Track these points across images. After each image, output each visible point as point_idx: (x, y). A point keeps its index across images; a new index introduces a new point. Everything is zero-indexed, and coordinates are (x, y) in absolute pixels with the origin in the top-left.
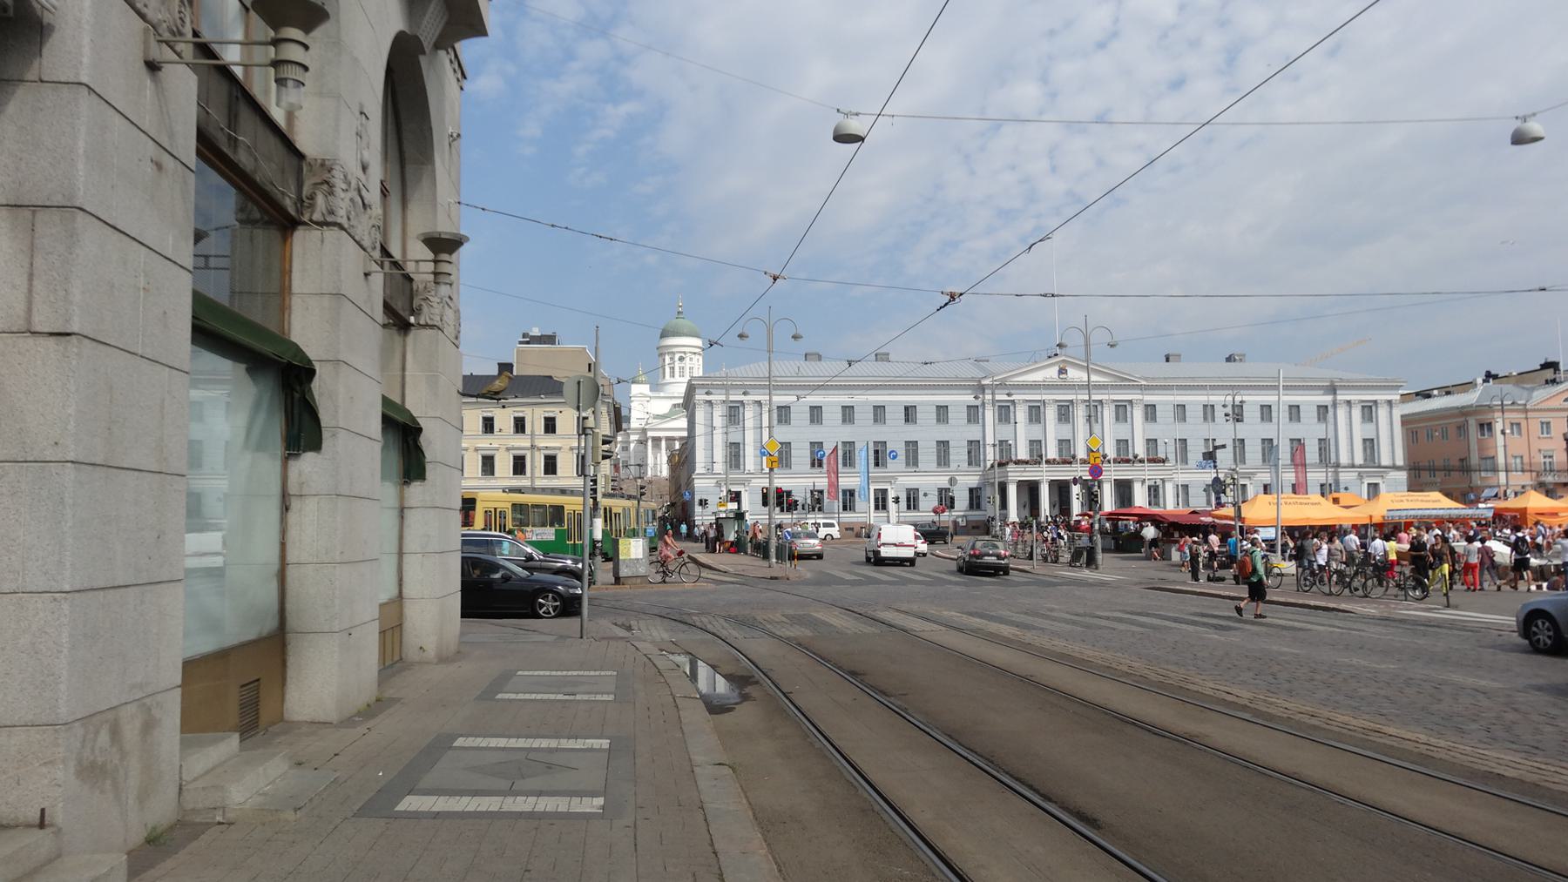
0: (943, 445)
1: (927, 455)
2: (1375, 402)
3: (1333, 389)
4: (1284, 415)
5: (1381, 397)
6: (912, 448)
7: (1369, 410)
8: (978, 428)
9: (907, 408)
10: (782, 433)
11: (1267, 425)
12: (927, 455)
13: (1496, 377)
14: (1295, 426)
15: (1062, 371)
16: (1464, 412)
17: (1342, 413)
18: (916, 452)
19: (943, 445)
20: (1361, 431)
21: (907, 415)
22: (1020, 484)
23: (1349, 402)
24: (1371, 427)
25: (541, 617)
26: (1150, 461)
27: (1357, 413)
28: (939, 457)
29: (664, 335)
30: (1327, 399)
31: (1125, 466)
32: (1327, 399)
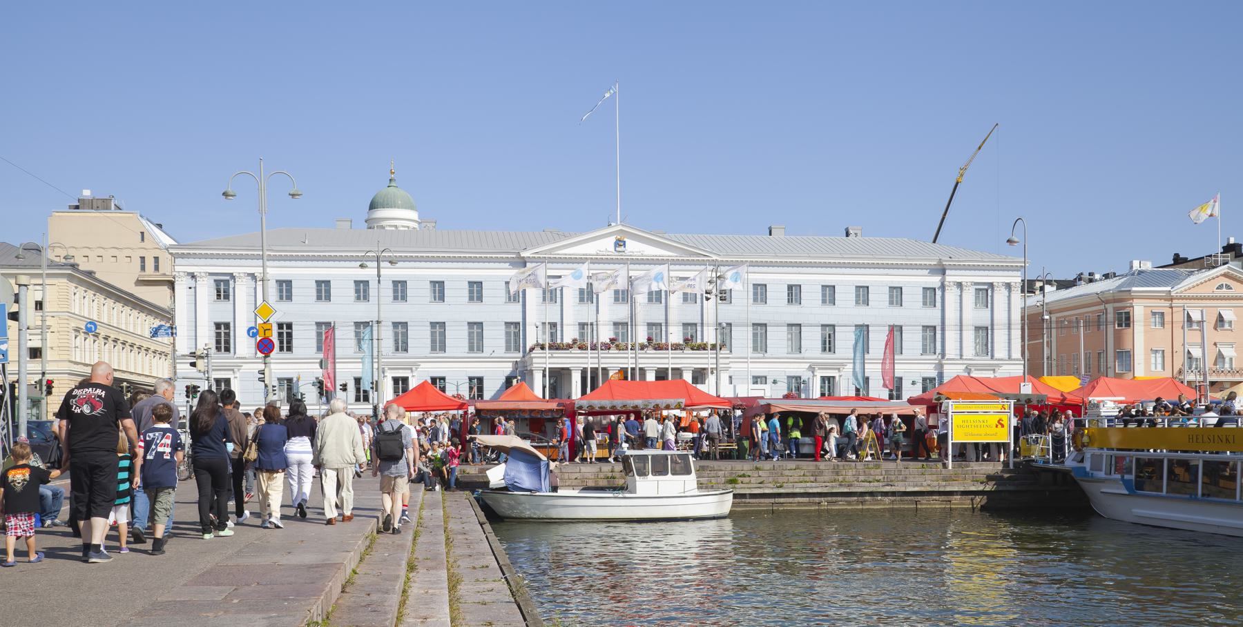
0: (476, 327)
1: (457, 338)
2: (991, 285)
3: (942, 271)
4: (388, 290)
5: (998, 278)
6: (438, 330)
7: (985, 293)
8: (228, 305)
9: (790, 287)
10: (282, 312)
11: (362, 306)
12: (457, 338)
13: (1185, 260)
14: (400, 306)
15: (619, 243)
16: (1102, 299)
17: (951, 296)
18: (443, 335)
19: (476, 327)
20: (975, 315)
21: (790, 294)
22: (823, 379)
23: (960, 285)
24: (226, 306)
25: (311, 521)
26: (551, 347)
27: (969, 296)
28: (433, 342)
29: (373, 206)
30: (935, 281)
31: (557, 353)
32: (935, 281)
